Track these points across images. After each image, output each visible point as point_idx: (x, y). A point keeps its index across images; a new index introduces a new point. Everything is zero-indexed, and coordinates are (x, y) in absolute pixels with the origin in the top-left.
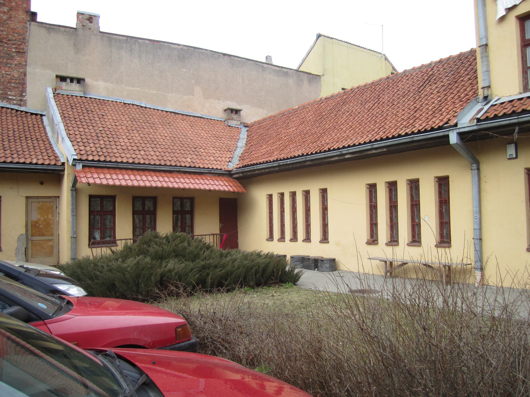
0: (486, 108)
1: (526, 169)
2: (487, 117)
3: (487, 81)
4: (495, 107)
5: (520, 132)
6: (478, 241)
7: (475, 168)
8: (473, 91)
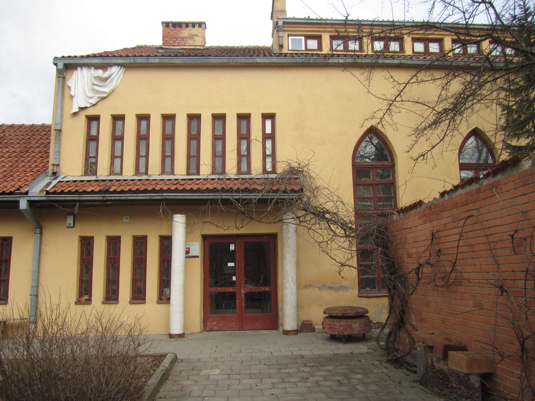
0: (54, 182)
1: (80, 237)
2: (55, 191)
3: (57, 160)
4: (62, 184)
5: (80, 206)
6: (35, 297)
7: (39, 232)
8: (43, 164)
